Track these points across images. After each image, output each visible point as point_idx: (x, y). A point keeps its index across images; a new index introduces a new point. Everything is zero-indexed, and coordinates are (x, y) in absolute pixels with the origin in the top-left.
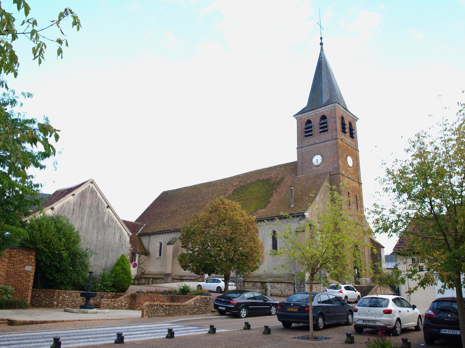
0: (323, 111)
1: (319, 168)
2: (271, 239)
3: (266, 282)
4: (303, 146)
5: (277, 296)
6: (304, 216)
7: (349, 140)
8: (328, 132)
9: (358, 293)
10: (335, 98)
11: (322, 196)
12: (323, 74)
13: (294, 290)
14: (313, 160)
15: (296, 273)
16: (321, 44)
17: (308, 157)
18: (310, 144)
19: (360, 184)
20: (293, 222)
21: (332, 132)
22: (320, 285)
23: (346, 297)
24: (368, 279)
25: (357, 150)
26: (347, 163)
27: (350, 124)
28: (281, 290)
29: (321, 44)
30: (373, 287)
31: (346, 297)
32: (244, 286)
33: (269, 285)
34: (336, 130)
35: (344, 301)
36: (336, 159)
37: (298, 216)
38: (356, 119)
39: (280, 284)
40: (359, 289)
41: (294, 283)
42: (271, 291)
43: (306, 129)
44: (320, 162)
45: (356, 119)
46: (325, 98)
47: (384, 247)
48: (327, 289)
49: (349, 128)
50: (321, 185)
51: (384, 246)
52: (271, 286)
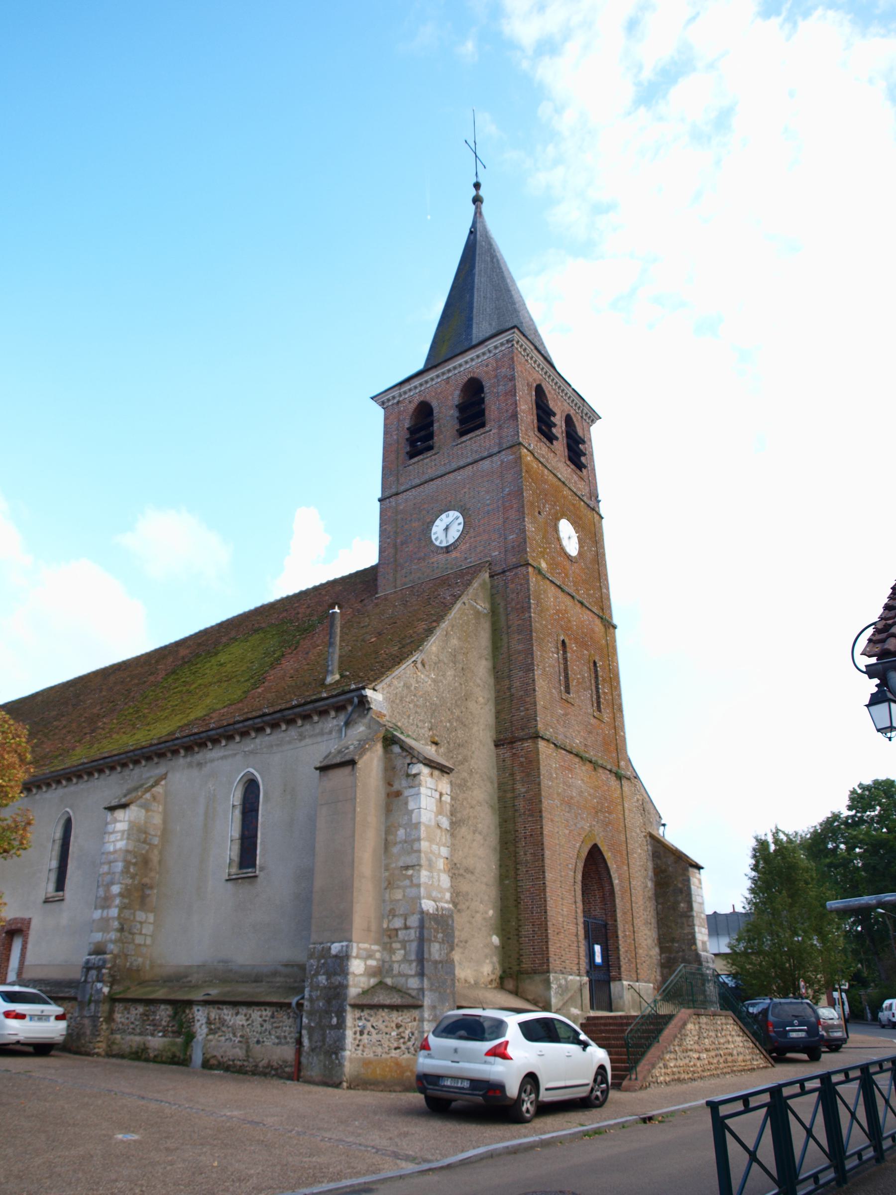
0: (468, 364)
1: (454, 554)
2: (238, 813)
3: (190, 1003)
4: (402, 488)
5: (227, 1069)
6: (363, 704)
8: (487, 429)
9: (598, 1055)
10: (513, 324)
11: (454, 642)
13: (299, 1042)
14: (434, 529)
15: (311, 956)
16: (477, 200)
17: (415, 524)
18: (427, 477)
19: (609, 626)
20: (322, 734)
21: (500, 427)
22: (416, 1013)
23: (531, 1079)
24: (647, 988)
27: (569, 420)
28: (245, 1040)
29: (477, 200)
30: (670, 1017)
31: (531, 1079)
32: (110, 1019)
33: (200, 1015)
34: (514, 416)
35: (519, 1101)
36: (513, 514)
37: (340, 708)
38: (592, 417)
39: (243, 1010)
40: (598, 1031)
41: (300, 1005)
43: (416, 431)
44: (455, 533)
45: (592, 417)
46: (481, 328)
47: (699, 868)
48: (433, 1040)
49: (565, 428)
50: (453, 604)
51: (701, 863)
52: (209, 1022)
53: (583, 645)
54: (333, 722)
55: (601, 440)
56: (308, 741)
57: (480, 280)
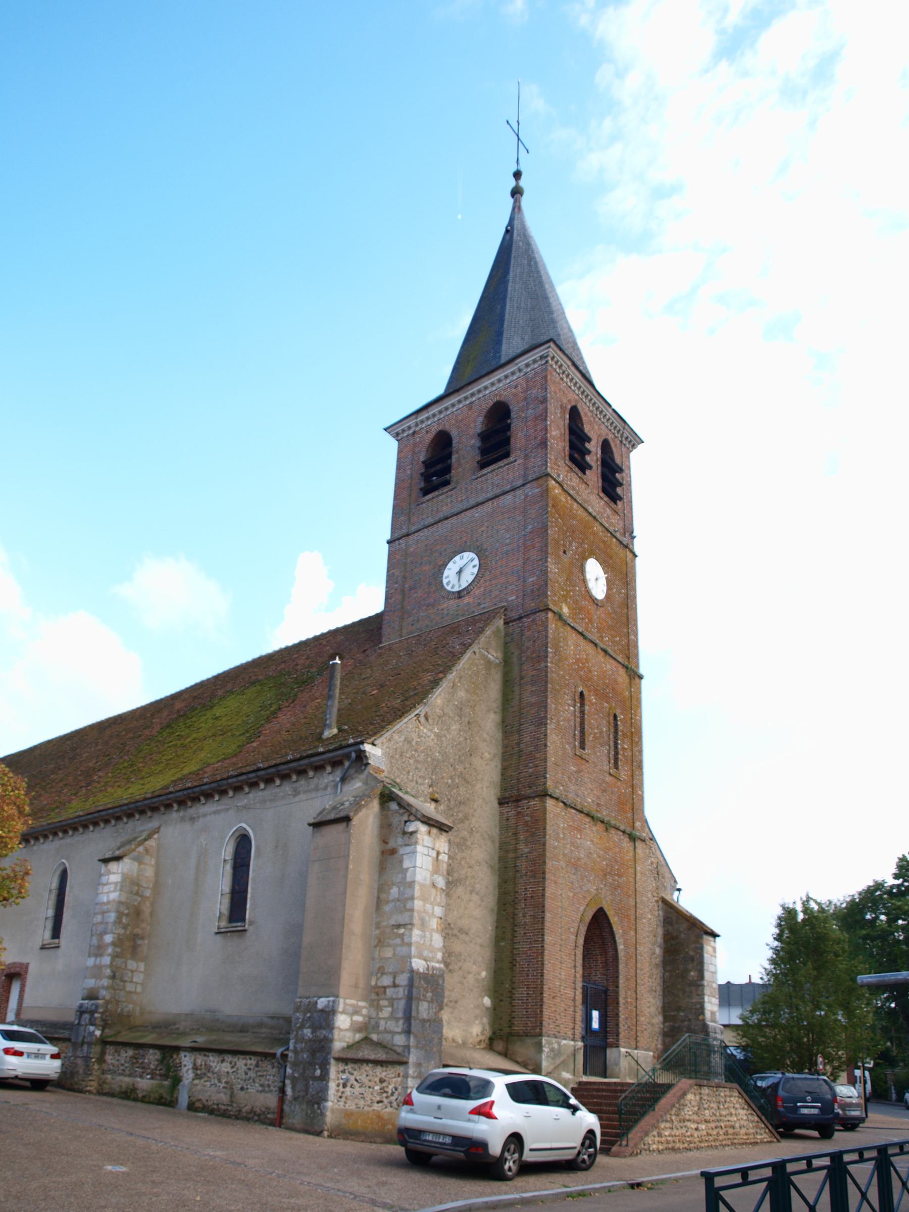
1: (466, 600)
2: (229, 868)
3: (177, 1049)
5: (211, 1112)
6: (361, 759)
7: (597, 503)
8: (511, 459)
9: (588, 1119)
10: (550, 337)
11: (462, 694)
12: (511, 274)
13: (282, 1091)
15: (297, 1009)
16: (516, 192)
19: (635, 676)
20: (317, 789)
21: (526, 457)
22: (400, 1069)
24: (646, 1057)
25: (628, 548)
26: (584, 581)
27: (606, 446)
28: (229, 1086)
29: (516, 192)
33: (187, 1061)
34: (544, 444)
36: (534, 554)
37: (336, 764)
38: (634, 440)
39: (229, 1058)
40: (588, 1096)
41: (284, 1056)
42: (192, 1085)
45: (634, 440)
46: (511, 344)
47: (714, 935)
48: (416, 1096)
51: (717, 930)
52: (195, 1068)
53: (603, 696)
54: (329, 777)
55: (642, 469)
56: (302, 796)
57: (514, 288)
